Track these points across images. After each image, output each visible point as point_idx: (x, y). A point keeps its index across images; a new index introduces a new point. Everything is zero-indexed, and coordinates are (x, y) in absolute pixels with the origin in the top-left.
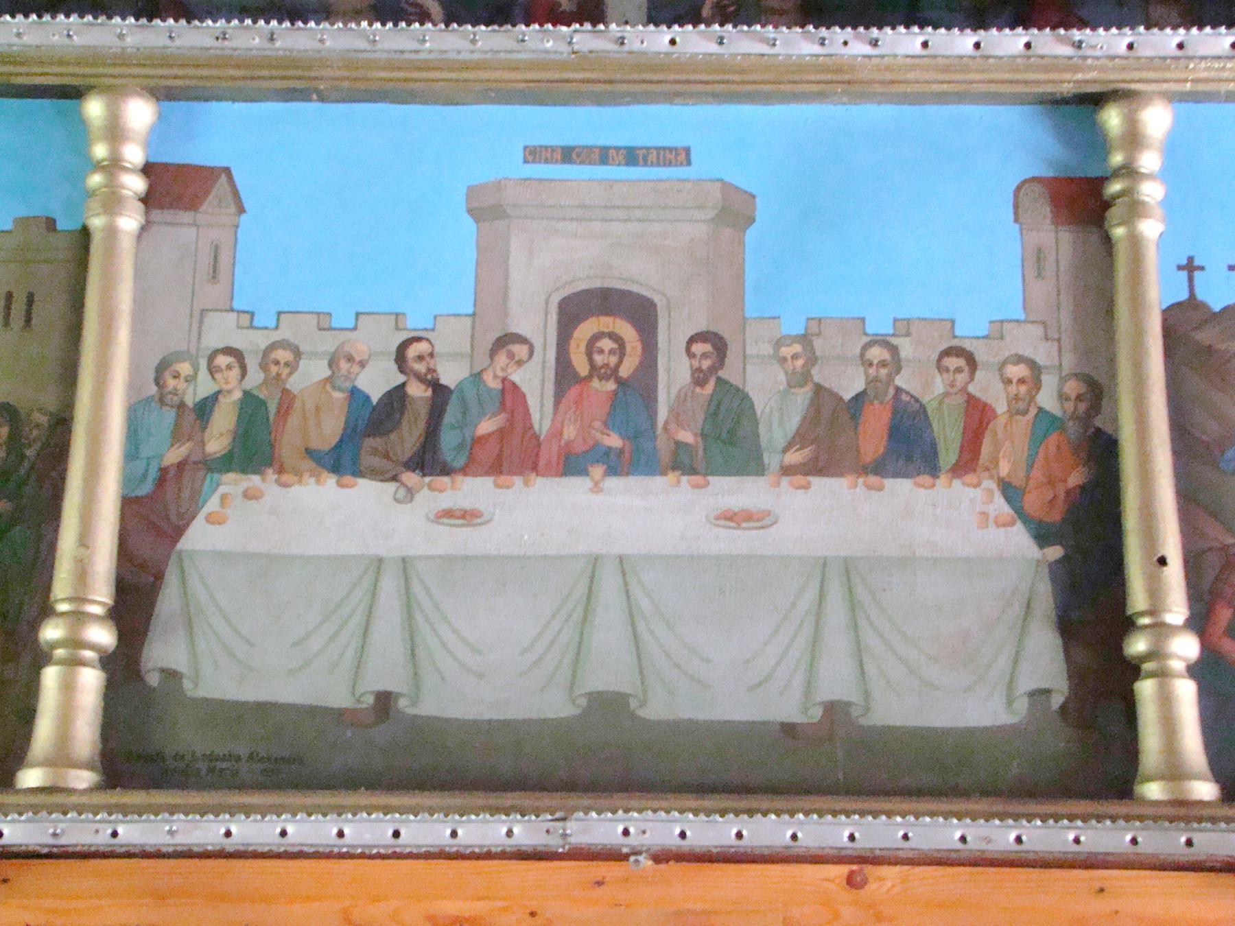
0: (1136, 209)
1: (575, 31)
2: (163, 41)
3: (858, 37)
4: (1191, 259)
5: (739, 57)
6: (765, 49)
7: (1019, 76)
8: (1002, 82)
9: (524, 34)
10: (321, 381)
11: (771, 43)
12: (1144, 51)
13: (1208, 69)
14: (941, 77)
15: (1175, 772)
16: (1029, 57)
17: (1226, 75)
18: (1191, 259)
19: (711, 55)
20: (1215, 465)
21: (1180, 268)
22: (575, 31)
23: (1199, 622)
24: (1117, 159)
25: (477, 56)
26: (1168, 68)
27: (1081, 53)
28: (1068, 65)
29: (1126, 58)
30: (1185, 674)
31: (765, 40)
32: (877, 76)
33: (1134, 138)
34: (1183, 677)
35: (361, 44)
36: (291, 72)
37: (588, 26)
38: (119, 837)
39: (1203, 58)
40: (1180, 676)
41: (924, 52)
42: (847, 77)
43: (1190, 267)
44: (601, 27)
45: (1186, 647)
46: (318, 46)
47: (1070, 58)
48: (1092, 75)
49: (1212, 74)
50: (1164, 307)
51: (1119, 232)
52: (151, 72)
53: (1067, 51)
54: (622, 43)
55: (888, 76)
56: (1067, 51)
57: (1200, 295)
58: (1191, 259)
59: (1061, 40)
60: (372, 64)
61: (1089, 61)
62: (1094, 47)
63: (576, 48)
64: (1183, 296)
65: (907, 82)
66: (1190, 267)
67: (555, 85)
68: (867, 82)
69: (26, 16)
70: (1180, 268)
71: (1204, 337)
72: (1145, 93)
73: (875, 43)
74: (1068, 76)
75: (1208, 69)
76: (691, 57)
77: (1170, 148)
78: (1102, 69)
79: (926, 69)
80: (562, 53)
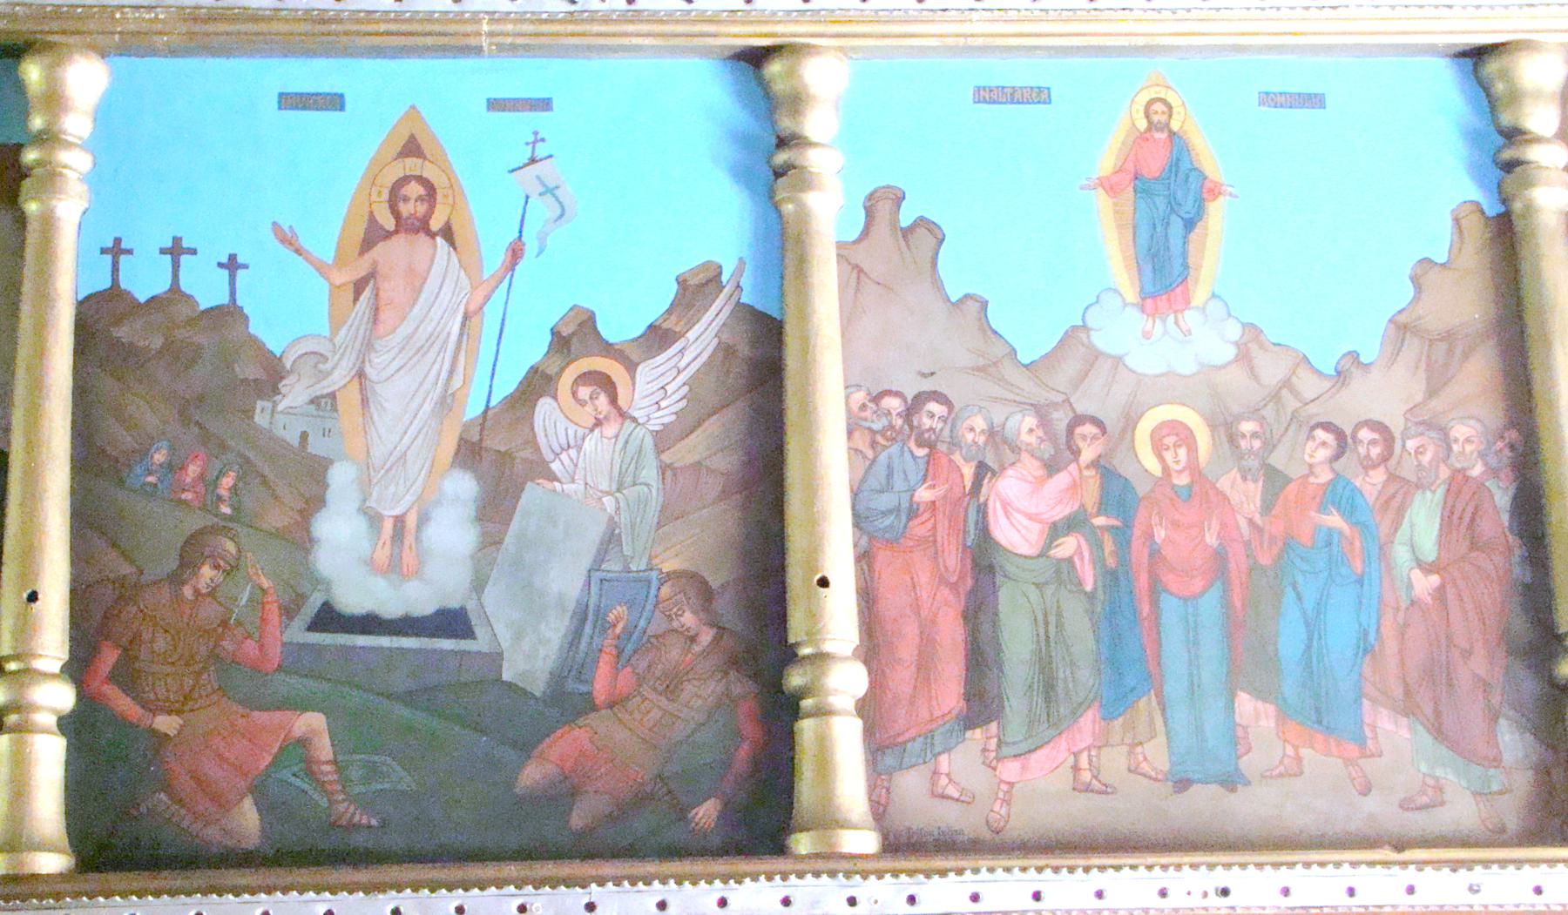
0: (51, 178)
4: (118, 241)
5: (393, 14)
8: (864, 36)
10: (838, 262)
15: (829, 821)
16: (749, 12)
18: (118, 241)
19: (447, 13)
20: (121, 483)
21: (104, 251)
23: (78, 668)
24: (37, 123)
30: (55, 729)
33: (55, 100)
34: (51, 733)
36: (334, 26)
38: (822, 589)
40: (47, 731)
43: (116, 251)
45: (57, 697)
50: (81, 297)
51: (32, 207)
57: (124, 284)
58: (177, 241)
64: (104, 283)
66: (116, 251)
70: (104, 251)
71: (123, 333)
72: (814, 46)
77: (102, 115)
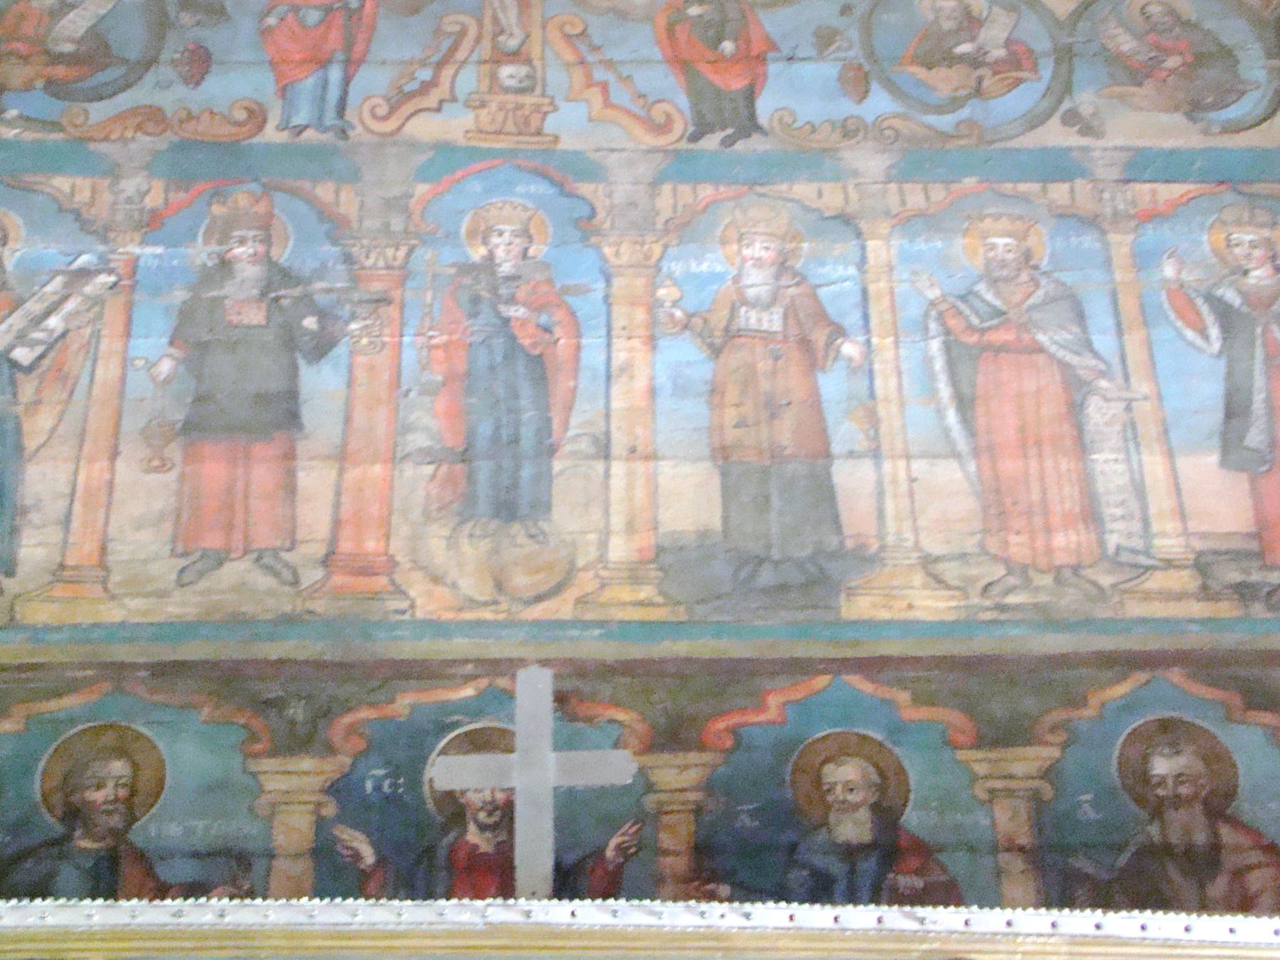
1: (489, 905)
2: (125, 919)
3: (733, 910)
6: (653, 921)
7: (872, 946)
9: (444, 908)
11: (396, 911)
12: (1063, 929)
13: (1034, 943)
14: (805, 945)
16: (881, 930)
17: (1049, 948)
22: (489, 905)
25: (402, 927)
26: (999, 941)
27: (924, 927)
28: (913, 937)
29: (963, 933)
31: (652, 913)
32: (753, 944)
35: (302, 919)
37: (499, 901)
39: (1029, 935)
41: (791, 924)
42: (725, 944)
44: (511, 901)
46: (262, 920)
47: (916, 932)
48: (936, 945)
49: (1038, 948)
52: (112, 945)
53: (914, 926)
54: (529, 917)
55: (761, 944)
56: (914, 926)
59: (908, 915)
60: (312, 935)
61: (932, 935)
62: (935, 923)
63: (489, 919)
65: (778, 949)
67: (471, 951)
68: (741, 949)
69: (322, 899)
73: (747, 916)
74: (915, 946)
75: (1034, 943)
76: (727, 928)
78: (944, 941)
79: (793, 938)
80: (477, 925)
